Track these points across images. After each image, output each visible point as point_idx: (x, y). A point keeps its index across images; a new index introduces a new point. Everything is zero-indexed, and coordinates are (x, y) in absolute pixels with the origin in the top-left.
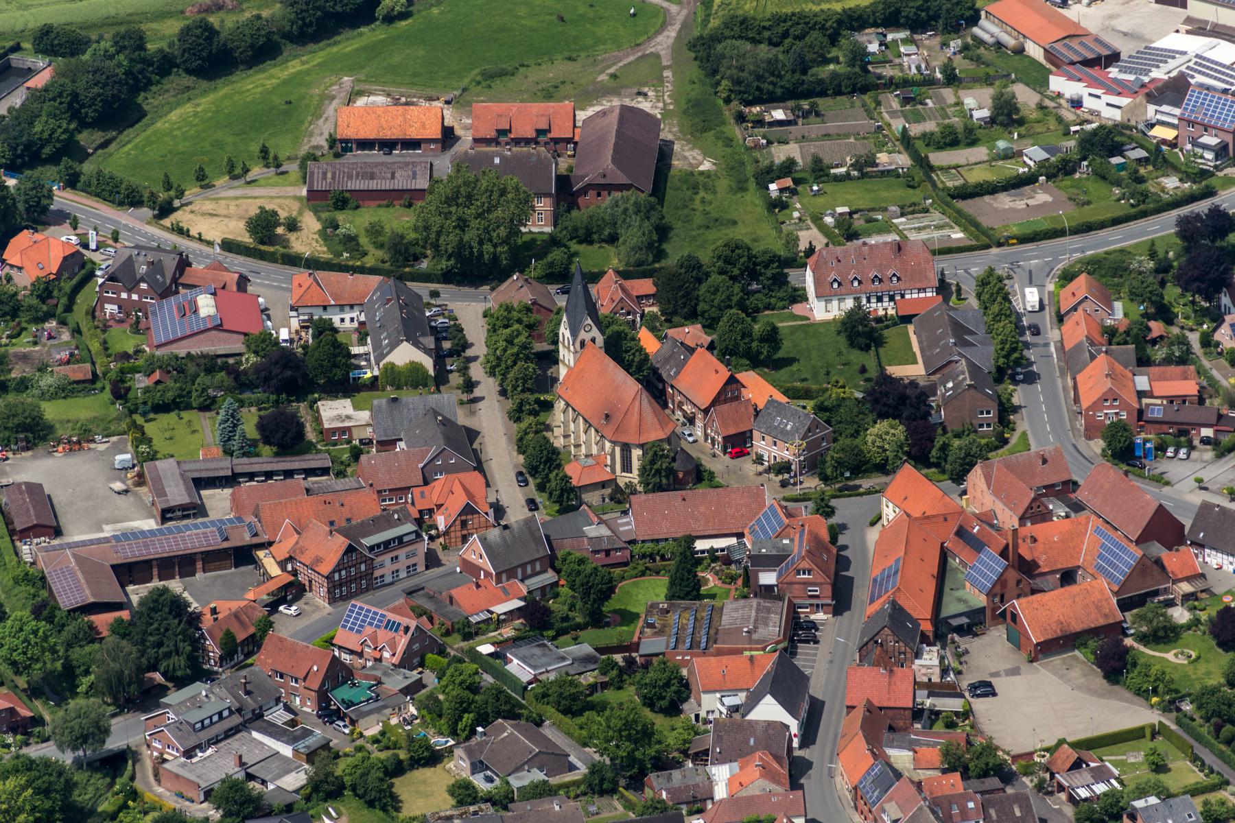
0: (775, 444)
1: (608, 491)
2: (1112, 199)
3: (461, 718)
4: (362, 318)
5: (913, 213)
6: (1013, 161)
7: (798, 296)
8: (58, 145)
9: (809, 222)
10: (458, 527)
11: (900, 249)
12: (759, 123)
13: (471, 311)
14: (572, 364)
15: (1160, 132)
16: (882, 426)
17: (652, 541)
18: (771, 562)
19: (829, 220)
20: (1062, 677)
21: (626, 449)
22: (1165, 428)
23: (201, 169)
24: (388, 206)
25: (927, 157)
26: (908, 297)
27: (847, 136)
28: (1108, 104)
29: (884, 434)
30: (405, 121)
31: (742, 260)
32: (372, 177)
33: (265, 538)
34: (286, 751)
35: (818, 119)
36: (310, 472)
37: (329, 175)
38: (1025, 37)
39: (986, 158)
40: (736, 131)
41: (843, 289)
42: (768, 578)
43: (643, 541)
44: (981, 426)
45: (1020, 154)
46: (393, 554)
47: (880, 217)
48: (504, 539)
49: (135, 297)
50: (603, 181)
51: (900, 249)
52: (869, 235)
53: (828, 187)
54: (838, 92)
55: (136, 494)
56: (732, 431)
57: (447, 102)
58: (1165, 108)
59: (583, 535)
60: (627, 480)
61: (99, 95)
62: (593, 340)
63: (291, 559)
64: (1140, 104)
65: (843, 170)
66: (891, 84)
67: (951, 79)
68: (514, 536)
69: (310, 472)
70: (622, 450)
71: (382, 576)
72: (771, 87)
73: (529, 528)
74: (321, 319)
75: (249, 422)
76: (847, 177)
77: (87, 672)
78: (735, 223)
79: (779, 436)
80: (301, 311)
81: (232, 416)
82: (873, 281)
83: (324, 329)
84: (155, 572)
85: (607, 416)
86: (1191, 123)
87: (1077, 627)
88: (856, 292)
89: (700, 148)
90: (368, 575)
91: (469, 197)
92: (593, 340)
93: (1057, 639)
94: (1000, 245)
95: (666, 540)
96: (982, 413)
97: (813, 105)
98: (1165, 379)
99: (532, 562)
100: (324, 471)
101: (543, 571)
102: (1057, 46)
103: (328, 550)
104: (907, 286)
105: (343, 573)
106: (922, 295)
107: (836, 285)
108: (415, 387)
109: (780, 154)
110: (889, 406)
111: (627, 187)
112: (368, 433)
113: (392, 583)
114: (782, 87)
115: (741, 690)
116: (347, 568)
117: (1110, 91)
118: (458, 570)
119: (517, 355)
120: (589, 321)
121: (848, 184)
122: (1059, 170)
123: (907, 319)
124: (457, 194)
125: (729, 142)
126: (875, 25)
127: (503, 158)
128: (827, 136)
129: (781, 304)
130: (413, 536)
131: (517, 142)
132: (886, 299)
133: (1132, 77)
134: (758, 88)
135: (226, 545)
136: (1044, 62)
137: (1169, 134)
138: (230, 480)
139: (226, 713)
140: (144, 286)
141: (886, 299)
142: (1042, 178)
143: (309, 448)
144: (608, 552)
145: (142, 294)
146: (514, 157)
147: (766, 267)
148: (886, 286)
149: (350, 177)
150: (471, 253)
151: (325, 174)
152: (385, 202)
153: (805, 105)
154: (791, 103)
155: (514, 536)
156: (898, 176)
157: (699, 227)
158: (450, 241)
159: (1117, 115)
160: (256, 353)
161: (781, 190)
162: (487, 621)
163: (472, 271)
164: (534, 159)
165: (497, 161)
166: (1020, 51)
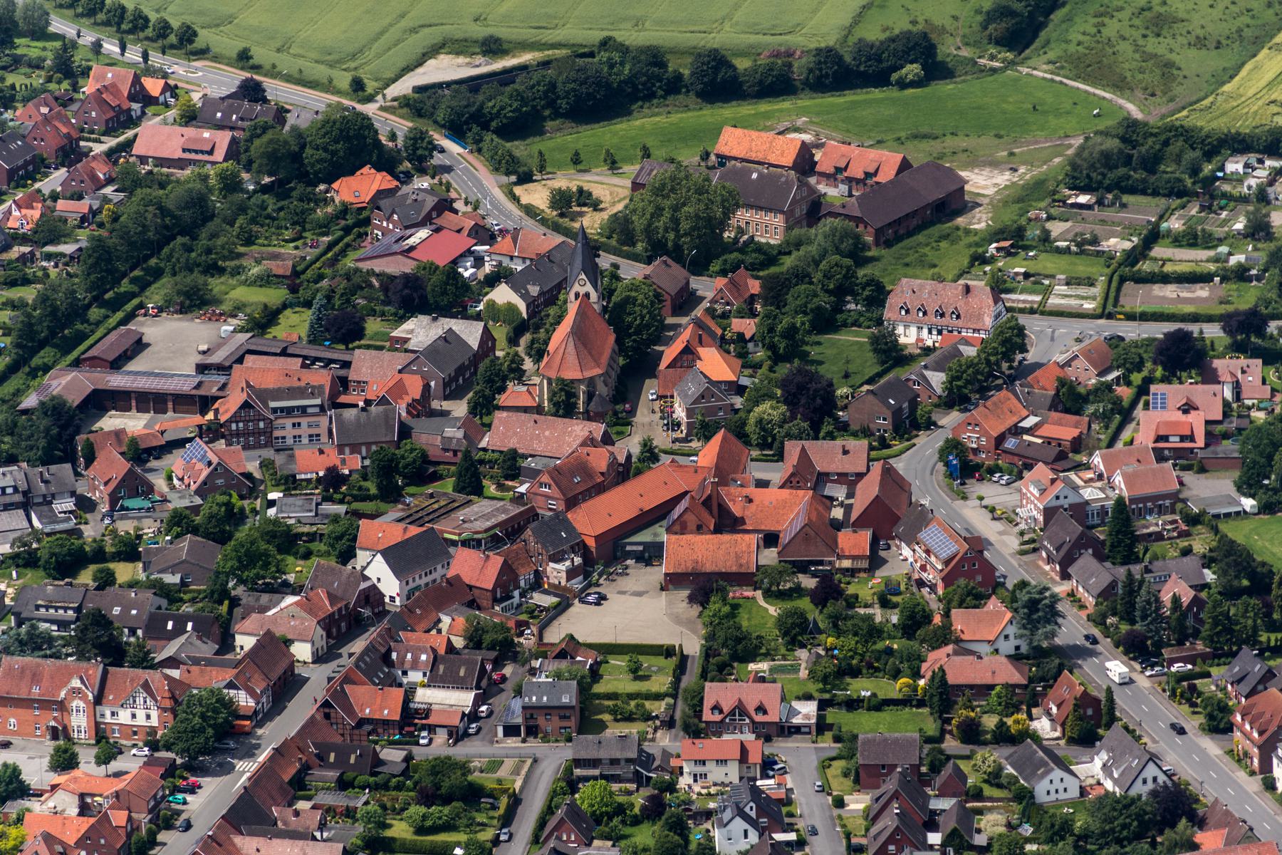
8: (505, 121)
22: (1016, 459)
23: (577, 154)
41: (909, 317)
43: (493, 451)
46: (296, 420)
50: (841, 211)
61: (574, 90)
68: (369, 418)
71: (284, 438)
76: (1067, 251)
80: (494, 257)
91: (673, 190)
93: (691, 574)
98: (1061, 424)
105: (241, 425)
116: (246, 422)
120: (583, 276)
121: (1066, 257)
124: (663, 185)
126: (1258, 151)
127: (760, 175)
132: (935, 332)
134: (1088, 176)
139: (9, 491)
142: (1217, 279)
146: (769, 174)
147: (864, 289)
148: (944, 321)
155: (369, 418)
164: (783, 179)
165: (755, 176)
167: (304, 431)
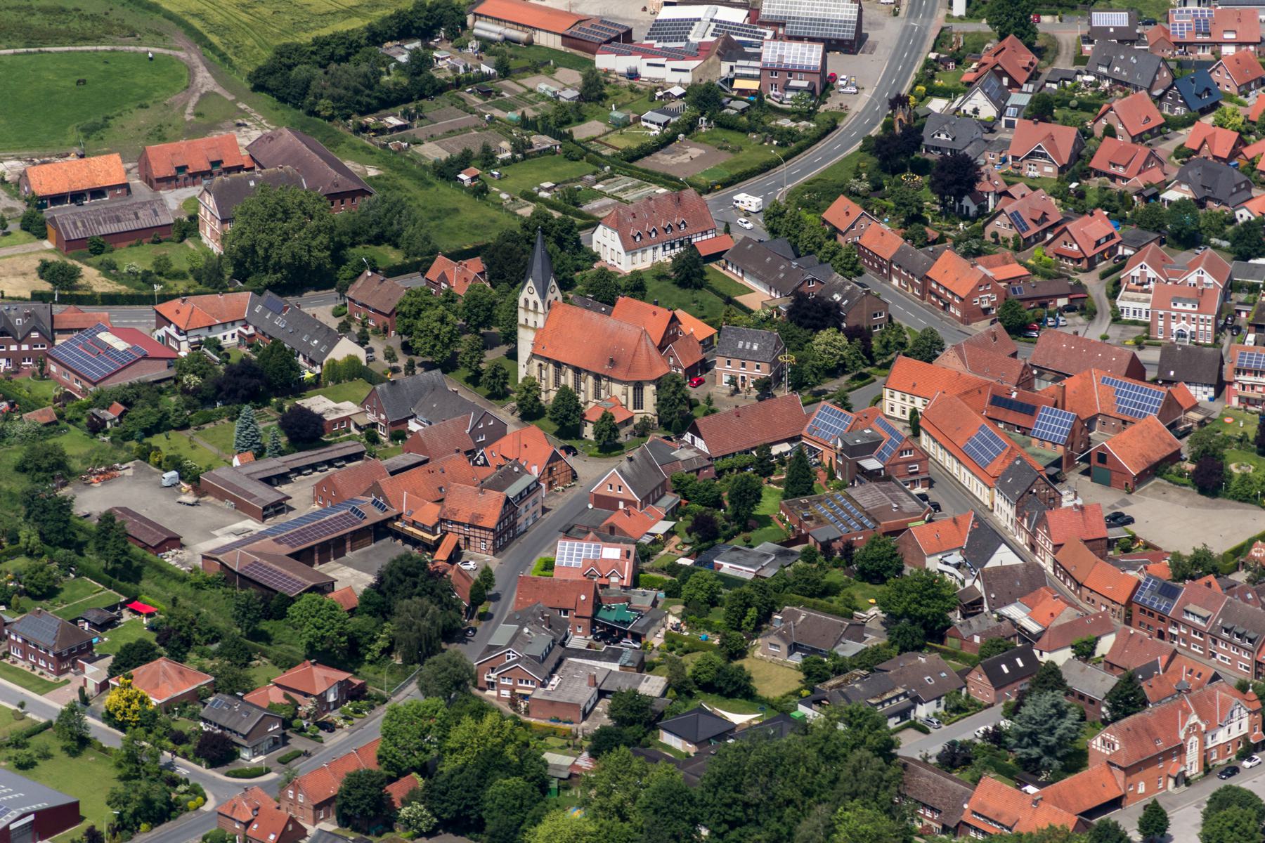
0: (743, 365)
1: (631, 427)
2: (754, 149)
3: (745, 614)
4: (251, 330)
5: (603, 179)
6: (634, 127)
7: (595, 257)
12: (381, 131)
13: (321, 308)
14: (541, 324)
15: (739, 84)
16: (825, 337)
17: (723, 457)
18: (870, 448)
20: (1167, 500)
21: (639, 387)
24: (137, 245)
25: (571, 132)
27: (467, 130)
28: (673, 70)
29: (827, 341)
30: (90, 171)
32: (119, 220)
33: (393, 512)
34: (615, 667)
35: (423, 121)
36: (349, 458)
37: (79, 224)
38: (534, 29)
39: (608, 129)
40: (364, 140)
42: (871, 464)
44: (875, 327)
45: (638, 120)
48: (632, 468)
49: (25, 347)
52: (587, 202)
53: (505, 171)
54: (422, 97)
55: (206, 503)
56: (690, 363)
57: (82, 156)
58: (740, 63)
59: (676, 460)
63: (442, 520)
64: (714, 63)
65: (508, 154)
66: (458, 84)
67: (505, 71)
69: (349, 458)
72: (368, 99)
74: (208, 339)
75: (267, 423)
76: (514, 160)
77: (373, 641)
78: (456, 210)
79: (745, 357)
81: (253, 422)
83: (217, 347)
84: (316, 557)
85: (612, 361)
86: (774, 71)
87: (1156, 458)
89: (350, 159)
90: (513, 525)
94: (709, 192)
95: (734, 454)
96: (875, 315)
97: (418, 110)
99: (657, 488)
100: (358, 456)
101: (663, 495)
102: (575, 30)
103: (489, 507)
106: (705, 237)
108: (351, 379)
109: (433, 152)
110: (817, 319)
111: (353, 194)
112: (371, 418)
113: (525, 531)
114: (376, 98)
115: (955, 549)
117: (670, 58)
118: (590, 506)
119: (451, 332)
122: (690, 128)
123: (716, 257)
125: (365, 148)
126: (391, 39)
128: (451, 132)
129: (587, 264)
131: (229, 170)
132: (677, 245)
133: (683, 44)
134: (359, 103)
135: (366, 523)
136: (563, 48)
137: (753, 85)
138: (283, 478)
140: (35, 335)
141: (677, 245)
142: (681, 136)
143: (328, 444)
144: (698, 471)
145: (33, 343)
148: (677, 233)
149: (99, 224)
150: (301, 261)
151: (75, 223)
152: (134, 242)
153: (412, 107)
154: (400, 109)
156: (555, 153)
157: (433, 219)
158: (284, 253)
159: (687, 78)
160: (194, 372)
161: (473, 179)
162: (655, 542)
163: (299, 279)
165: (252, 184)
166: (530, 43)
167: (532, 509)
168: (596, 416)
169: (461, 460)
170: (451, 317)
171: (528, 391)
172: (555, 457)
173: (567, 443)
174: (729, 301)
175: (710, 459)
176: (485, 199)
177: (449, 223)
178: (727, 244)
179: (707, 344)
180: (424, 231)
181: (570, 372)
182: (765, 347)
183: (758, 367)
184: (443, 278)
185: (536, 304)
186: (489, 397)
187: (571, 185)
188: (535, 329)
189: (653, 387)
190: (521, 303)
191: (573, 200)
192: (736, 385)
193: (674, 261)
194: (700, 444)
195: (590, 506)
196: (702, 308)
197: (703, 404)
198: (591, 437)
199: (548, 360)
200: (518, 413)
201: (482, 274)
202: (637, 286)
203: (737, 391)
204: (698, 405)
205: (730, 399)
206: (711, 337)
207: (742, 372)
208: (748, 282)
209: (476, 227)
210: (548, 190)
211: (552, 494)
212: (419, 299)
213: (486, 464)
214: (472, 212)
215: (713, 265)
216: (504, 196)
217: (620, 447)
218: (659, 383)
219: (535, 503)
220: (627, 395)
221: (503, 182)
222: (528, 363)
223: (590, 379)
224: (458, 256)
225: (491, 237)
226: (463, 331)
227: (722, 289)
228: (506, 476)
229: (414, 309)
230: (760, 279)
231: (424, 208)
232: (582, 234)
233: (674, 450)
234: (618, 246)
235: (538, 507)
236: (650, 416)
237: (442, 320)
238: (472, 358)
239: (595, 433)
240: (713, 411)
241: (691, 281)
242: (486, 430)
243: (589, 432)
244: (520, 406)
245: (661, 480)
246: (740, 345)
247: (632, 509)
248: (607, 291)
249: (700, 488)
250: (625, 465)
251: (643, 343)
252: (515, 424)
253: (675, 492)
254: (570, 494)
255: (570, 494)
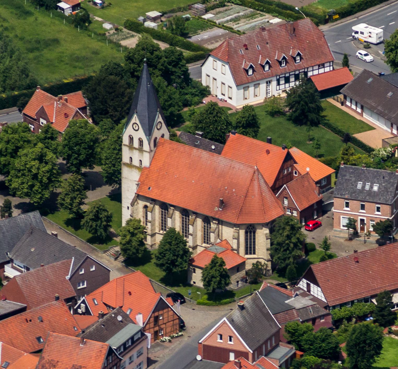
0: (363, 207)
1: (242, 274)
7: (205, 92)
9: (125, 30)
10: (152, 325)
11: (294, 29)
14: (146, 163)
17: (341, 305)
19: (150, 24)
21: (251, 230)
26: (310, 74)
31: (162, 61)
43: (334, 307)
47: (188, 15)
48: (244, 318)
51: (294, 29)
52: (195, 33)
56: (306, 205)
59: (291, 308)
60: (255, 261)
62: (163, 136)
70: (246, 233)
73: (257, 306)
78: (56, 41)
79: (364, 199)
82: (280, 63)
85: (222, 202)
88: (269, 76)
92: (163, 136)
95: (352, 302)
99: (270, 339)
101: (277, 346)
104: (309, 63)
106: (321, 71)
107: (250, 72)
118: (199, 358)
123: (333, 91)
129: (196, 99)
130: (139, 335)
141: (292, 79)
144: (314, 320)
161: (74, 8)
167: (137, 361)
168: (205, 262)
169: (60, 308)
170: (50, 155)
171: (133, 235)
172: (161, 305)
173: (174, 290)
174: (348, 138)
175: (327, 307)
176: (86, 29)
177: (48, 54)
178: (346, 77)
179: (324, 184)
180: (21, 64)
181: (177, 214)
182: (386, 188)
183: (378, 209)
184: (42, 113)
185: (141, 142)
186: (91, 241)
187: (179, 14)
188: (140, 168)
189: (266, 231)
190: (126, 140)
191: (180, 31)
192: (355, 228)
193: (289, 95)
194: (316, 291)
195: (199, 358)
196: (318, 146)
197: (319, 249)
198: (200, 284)
199: (154, 201)
200: (122, 258)
201: (83, 109)
202: (249, 123)
203: (356, 234)
204: (313, 249)
205: (348, 243)
206: (328, 178)
207: (361, 215)
208: (368, 118)
209: (78, 59)
210: (154, 19)
211: (158, 345)
212: (16, 136)
213: (87, 312)
214: (73, 43)
215: (330, 100)
216: (107, 26)
217: (231, 295)
218: (272, 226)
219: (140, 354)
220: (238, 239)
221: (106, 11)
222: (132, 204)
223: (199, 222)
224: (58, 90)
225: (93, 70)
226: (64, 170)
227: (339, 125)
228: (109, 326)
229: (11, 147)
230: (381, 115)
231: (22, 39)
232: (191, 67)
233: (289, 297)
234: (229, 80)
235: (143, 358)
236: (263, 262)
237: (41, 158)
238: (73, 199)
239: (204, 280)
240: (331, 257)
241: (306, 117)
242: (88, 276)
243: (197, 278)
244: (124, 250)
245: (274, 330)
246: (360, 186)
247: (243, 361)
248: (217, 128)
249: (316, 338)
250: (236, 314)
251: (256, 183)
252: (119, 270)
253: (289, 343)
254: (177, 345)
255: (177, 345)
